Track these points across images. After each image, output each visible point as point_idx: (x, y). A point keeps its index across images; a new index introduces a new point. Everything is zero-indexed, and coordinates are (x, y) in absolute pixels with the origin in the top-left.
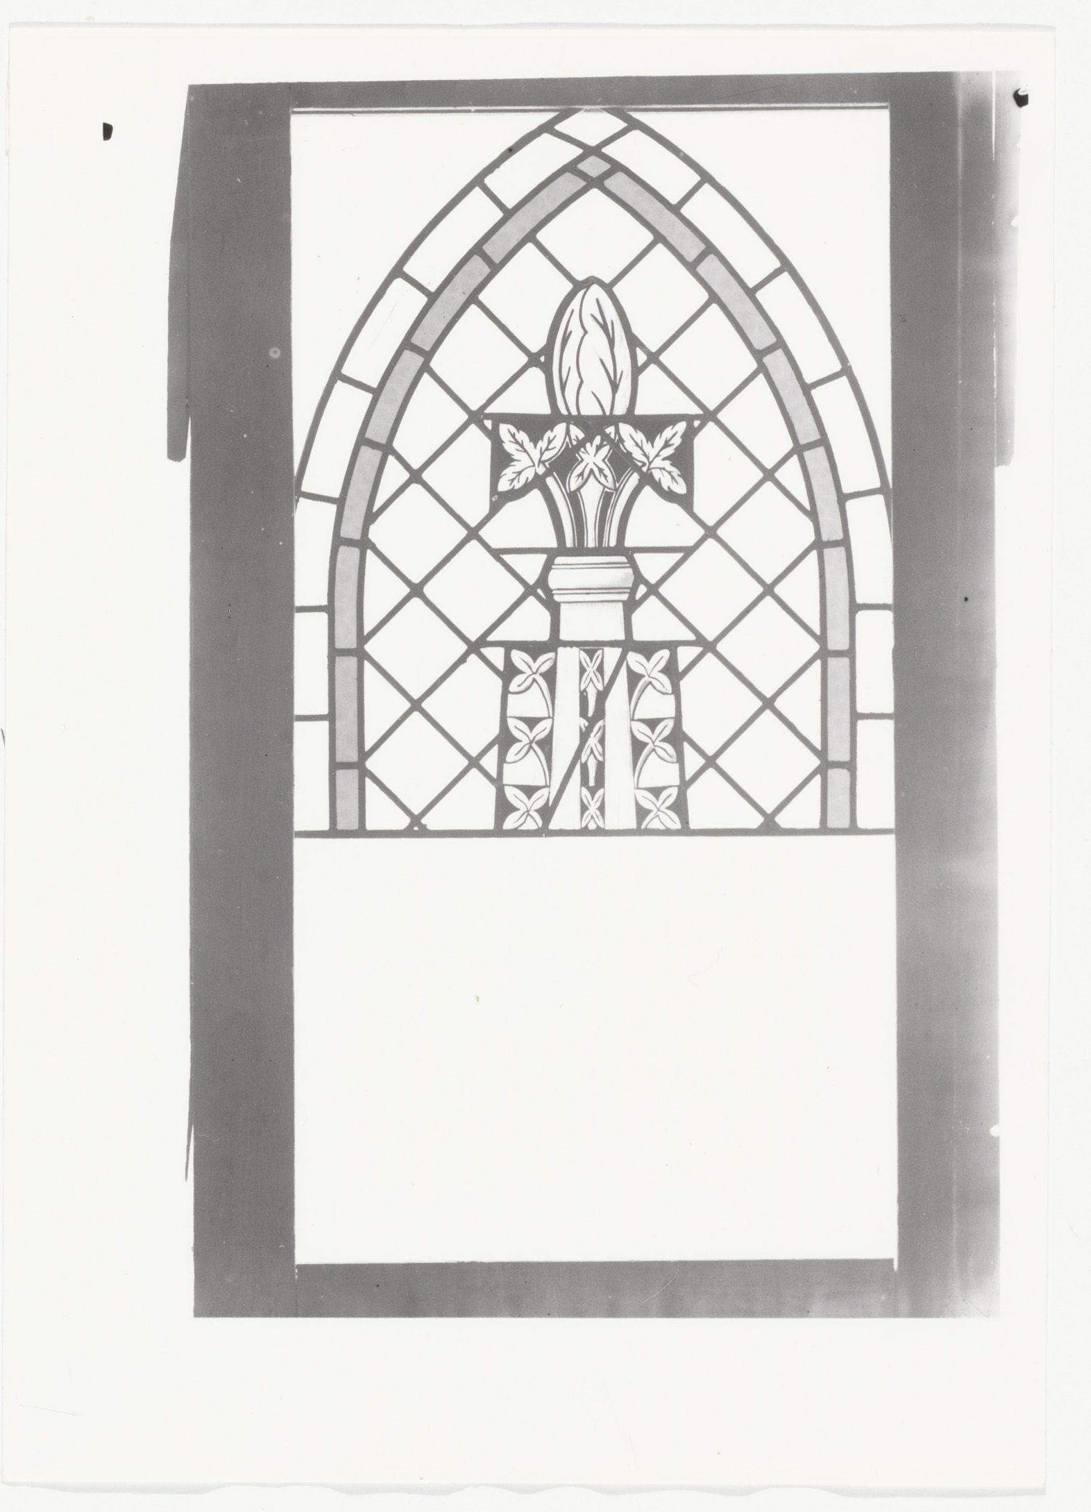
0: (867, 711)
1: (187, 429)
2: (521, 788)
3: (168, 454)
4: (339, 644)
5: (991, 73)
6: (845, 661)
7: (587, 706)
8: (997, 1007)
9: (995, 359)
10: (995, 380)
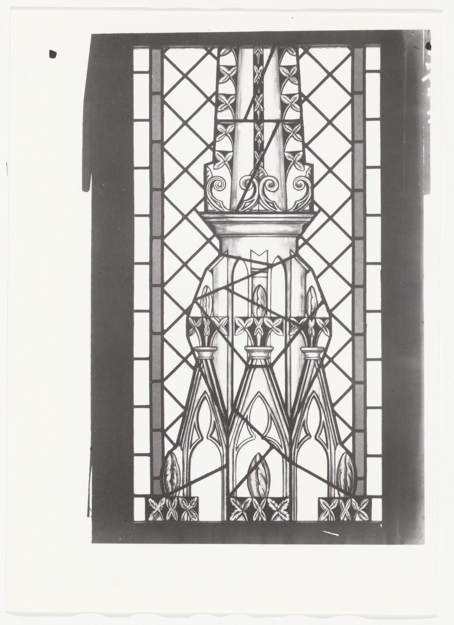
0: (372, 453)
1: (90, 179)
2: (232, 160)
3: (83, 188)
4: (154, 282)
5: (422, 30)
6: (362, 338)
7: (255, 431)
8: (423, 467)
9: (424, 150)
10: (424, 159)
